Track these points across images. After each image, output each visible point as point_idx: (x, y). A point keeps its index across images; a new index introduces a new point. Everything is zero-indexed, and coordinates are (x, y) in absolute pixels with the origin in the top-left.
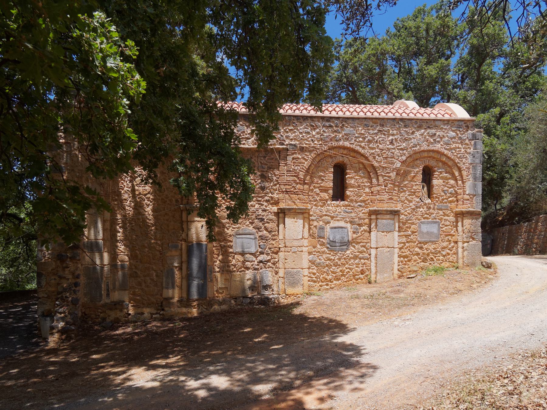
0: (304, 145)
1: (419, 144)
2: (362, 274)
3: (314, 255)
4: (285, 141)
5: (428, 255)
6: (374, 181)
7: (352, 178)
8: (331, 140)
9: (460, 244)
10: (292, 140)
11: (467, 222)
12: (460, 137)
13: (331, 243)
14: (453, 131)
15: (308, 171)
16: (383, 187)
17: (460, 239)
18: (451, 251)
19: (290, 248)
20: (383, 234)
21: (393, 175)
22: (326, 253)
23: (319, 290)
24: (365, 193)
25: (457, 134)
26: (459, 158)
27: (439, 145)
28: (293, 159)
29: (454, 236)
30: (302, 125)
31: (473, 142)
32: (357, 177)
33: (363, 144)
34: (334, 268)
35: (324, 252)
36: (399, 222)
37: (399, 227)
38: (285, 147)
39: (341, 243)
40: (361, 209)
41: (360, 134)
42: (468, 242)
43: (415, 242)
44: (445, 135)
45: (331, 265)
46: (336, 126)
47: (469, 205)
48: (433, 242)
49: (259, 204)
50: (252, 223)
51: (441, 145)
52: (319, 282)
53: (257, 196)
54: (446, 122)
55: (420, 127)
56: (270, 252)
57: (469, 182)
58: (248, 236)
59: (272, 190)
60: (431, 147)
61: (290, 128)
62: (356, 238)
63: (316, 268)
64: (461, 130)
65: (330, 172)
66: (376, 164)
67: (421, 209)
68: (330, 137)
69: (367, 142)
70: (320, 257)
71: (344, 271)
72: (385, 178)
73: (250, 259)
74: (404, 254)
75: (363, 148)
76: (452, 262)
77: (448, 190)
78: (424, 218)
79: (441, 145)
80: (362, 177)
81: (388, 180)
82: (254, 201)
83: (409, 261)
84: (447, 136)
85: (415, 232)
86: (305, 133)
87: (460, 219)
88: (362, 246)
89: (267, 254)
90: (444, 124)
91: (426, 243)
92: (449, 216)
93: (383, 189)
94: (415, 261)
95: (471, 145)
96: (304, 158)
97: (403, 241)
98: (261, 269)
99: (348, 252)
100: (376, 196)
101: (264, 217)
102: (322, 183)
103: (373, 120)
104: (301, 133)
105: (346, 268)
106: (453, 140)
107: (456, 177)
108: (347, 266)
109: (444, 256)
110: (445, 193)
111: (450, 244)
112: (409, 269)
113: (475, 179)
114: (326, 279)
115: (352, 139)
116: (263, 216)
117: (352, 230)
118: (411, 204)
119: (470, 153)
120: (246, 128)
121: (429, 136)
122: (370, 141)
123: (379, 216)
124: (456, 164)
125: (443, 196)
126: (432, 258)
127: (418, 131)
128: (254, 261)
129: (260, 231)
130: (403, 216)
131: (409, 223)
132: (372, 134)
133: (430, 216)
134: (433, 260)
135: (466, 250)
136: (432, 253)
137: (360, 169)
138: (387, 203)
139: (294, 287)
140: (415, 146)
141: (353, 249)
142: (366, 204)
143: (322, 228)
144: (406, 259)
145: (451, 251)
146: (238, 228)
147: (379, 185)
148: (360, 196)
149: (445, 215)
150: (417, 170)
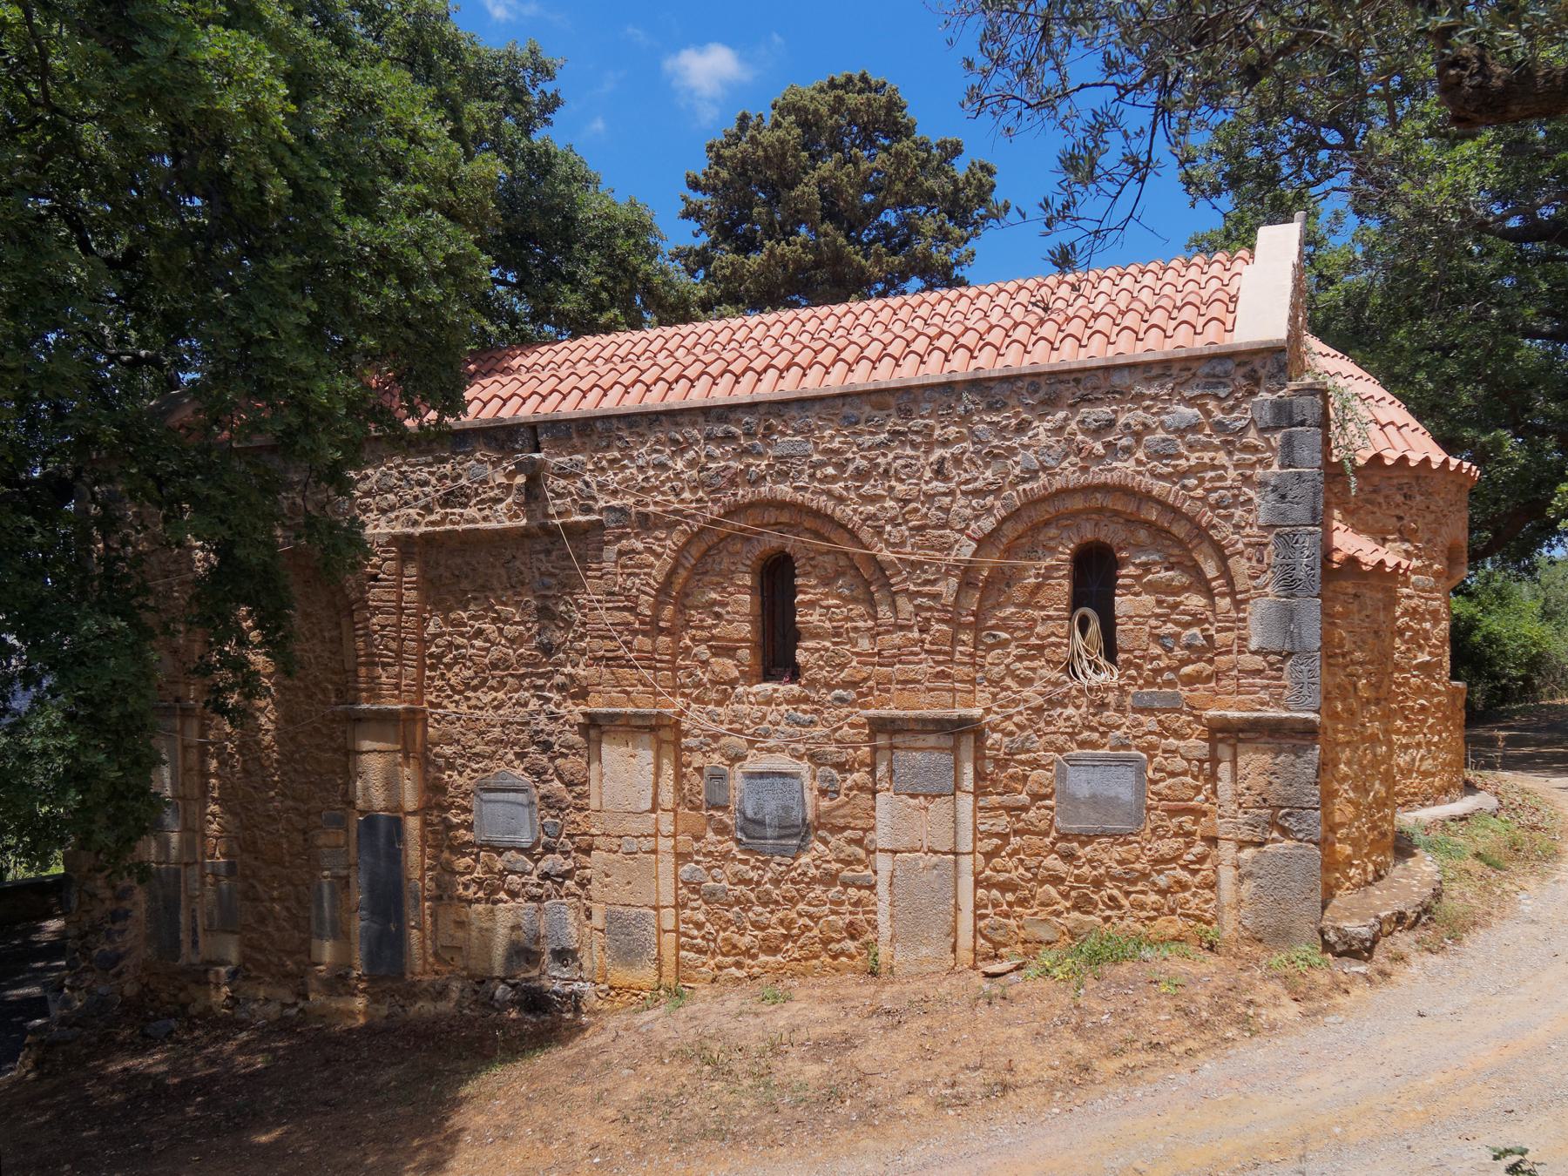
0: (652, 508)
1: (1044, 469)
2: (853, 938)
3: (697, 863)
4: (593, 498)
5: (1098, 884)
6: (884, 612)
7: (811, 604)
8: (732, 483)
9: (1227, 850)
10: (614, 493)
11: (1255, 762)
12: (1220, 423)
13: (751, 827)
14: (1189, 402)
15: (664, 589)
16: (916, 634)
17: (1222, 828)
18: (1194, 872)
19: (614, 840)
20: (912, 802)
21: (947, 588)
22: (734, 858)
23: (714, 980)
24: (858, 654)
25: (1208, 414)
26: (1213, 508)
27: (1132, 462)
28: (621, 553)
29: (1205, 814)
30: (644, 444)
31: (1277, 439)
32: (832, 602)
33: (837, 487)
34: (759, 909)
35: (726, 856)
36: (979, 758)
37: (979, 776)
38: (595, 517)
39: (781, 827)
40: (845, 711)
41: (826, 451)
42: (1261, 844)
43: (1047, 834)
44: (1152, 421)
45: (749, 901)
46: (749, 434)
47: (1264, 695)
48: (1117, 837)
49: (539, 698)
50: (521, 756)
51: (1139, 462)
52: (714, 953)
53: (531, 675)
54: (1154, 372)
55: (1051, 403)
56: (570, 846)
57: (1262, 603)
58: (512, 796)
59: (573, 655)
60: (1097, 475)
61: (609, 456)
62: (829, 812)
63: (704, 907)
64: (1222, 393)
65: (741, 589)
66: (886, 554)
67: (1070, 711)
68: (728, 474)
69: (852, 477)
70: (714, 872)
71: (792, 921)
72: (919, 601)
73: (519, 867)
74: (1003, 877)
75: (841, 500)
76: (1199, 919)
77: (1176, 636)
78: (1082, 744)
79: (1139, 462)
80: (846, 600)
81: (930, 609)
82: (526, 690)
83: (1022, 902)
84: (1162, 423)
85: (1047, 797)
86: (655, 467)
87: (1224, 751)
88: (851, 841)
89: (562, 853)
90: (1149, 381)
91: (1087, 839)
92: (1183, 737)
93: (915, 642)
94: (1042, 904)
95: (1273, 449)
96: (650, 550)
97: (996, 829)
98: (549, 897)
99: (805, 859)
100: (892, 665)
101: (552, 739)
102: (715, 626)
103: (873, 398)
104: (640, 469)
105: (800, 915)
106: (1190, 437)
107: (1208, 582)
108: (801, 906)
109: (1163, 892)
110: (1163, 646)
111: (1189, 845)
112: (1022, 934)
113: (1290, 585)
114: (735, 947)
115: (800, 472)
116: (549, 735)
117: (817, 784)
118: (1027, 692)
119: (1263, 484)
120: (490, 467)
121: (1084, 432)
122: (862, 475)
123: (898, 740)
124: (1202, 533)
125: (1158, 657)
126: (1111, 898)
127: (1042, 417)
128: (530, 874)
129: (545, 782)
130: (997, 736)
131: (1022, 763)
132: (870, 448)
133: (1104, 734)
134: (1120, 907)
135: (1250, 875)
136: (1113, 878)
137: (839, 574)
138: (930, 690)
139: (631, 965)
140: (1033, 475)
141: (821, 847)
142: (861, 695)
143: (719, 777)
144: (1010, 897)
145: (1194, 872)
146: (485, 771)
147: (902, 628)
148: (842, 667)
149: (1166, 731)
150: (1049, 561)
